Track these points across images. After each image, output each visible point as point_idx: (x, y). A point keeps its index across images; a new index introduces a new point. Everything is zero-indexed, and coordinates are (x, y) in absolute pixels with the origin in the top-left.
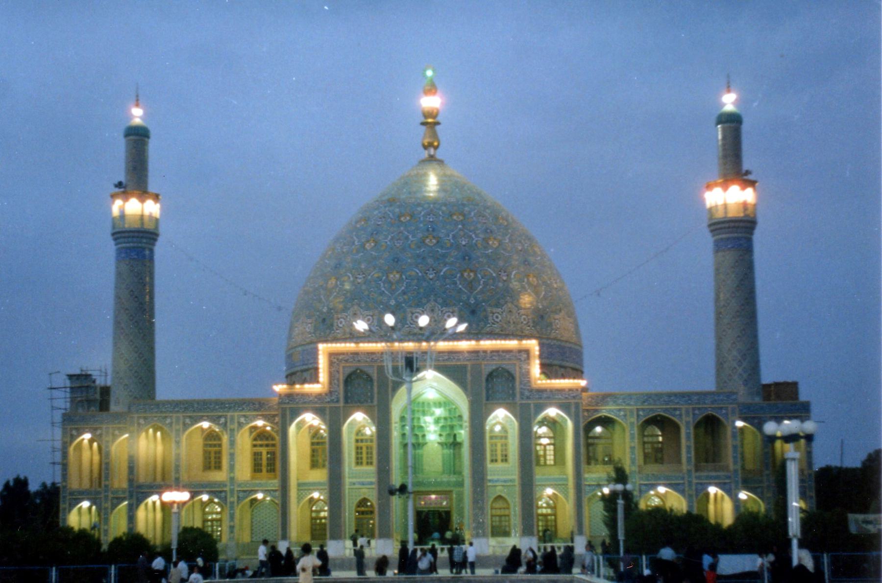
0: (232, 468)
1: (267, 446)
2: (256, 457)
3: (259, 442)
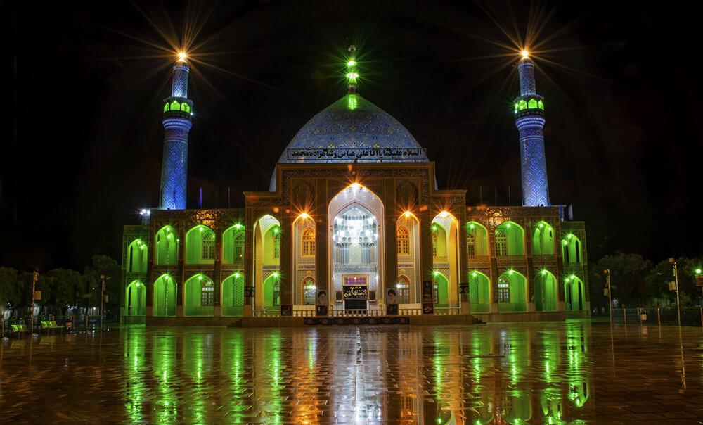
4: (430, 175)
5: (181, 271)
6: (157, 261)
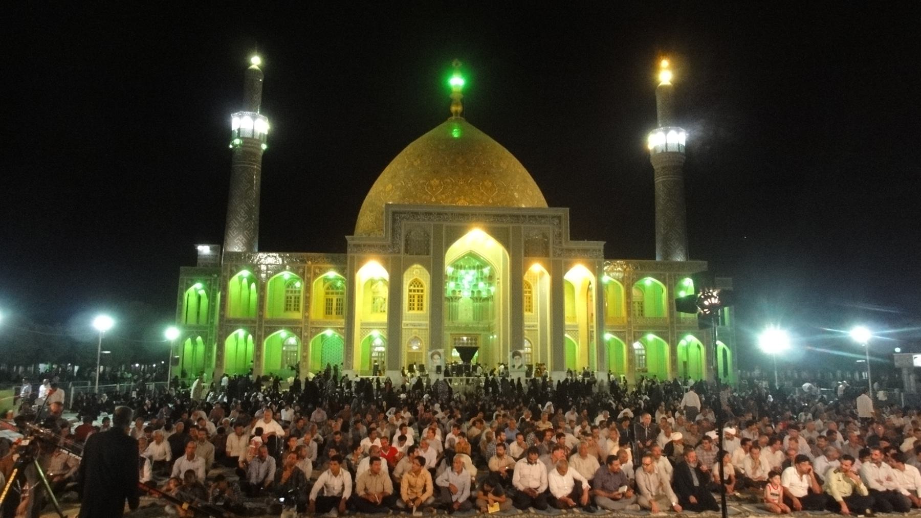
0: (307, 308)
1: (337, 293)
2: (329, 302)
3: (331, 291)
4: (563, 222)
5: (260, 326)
6: (268, 315)
